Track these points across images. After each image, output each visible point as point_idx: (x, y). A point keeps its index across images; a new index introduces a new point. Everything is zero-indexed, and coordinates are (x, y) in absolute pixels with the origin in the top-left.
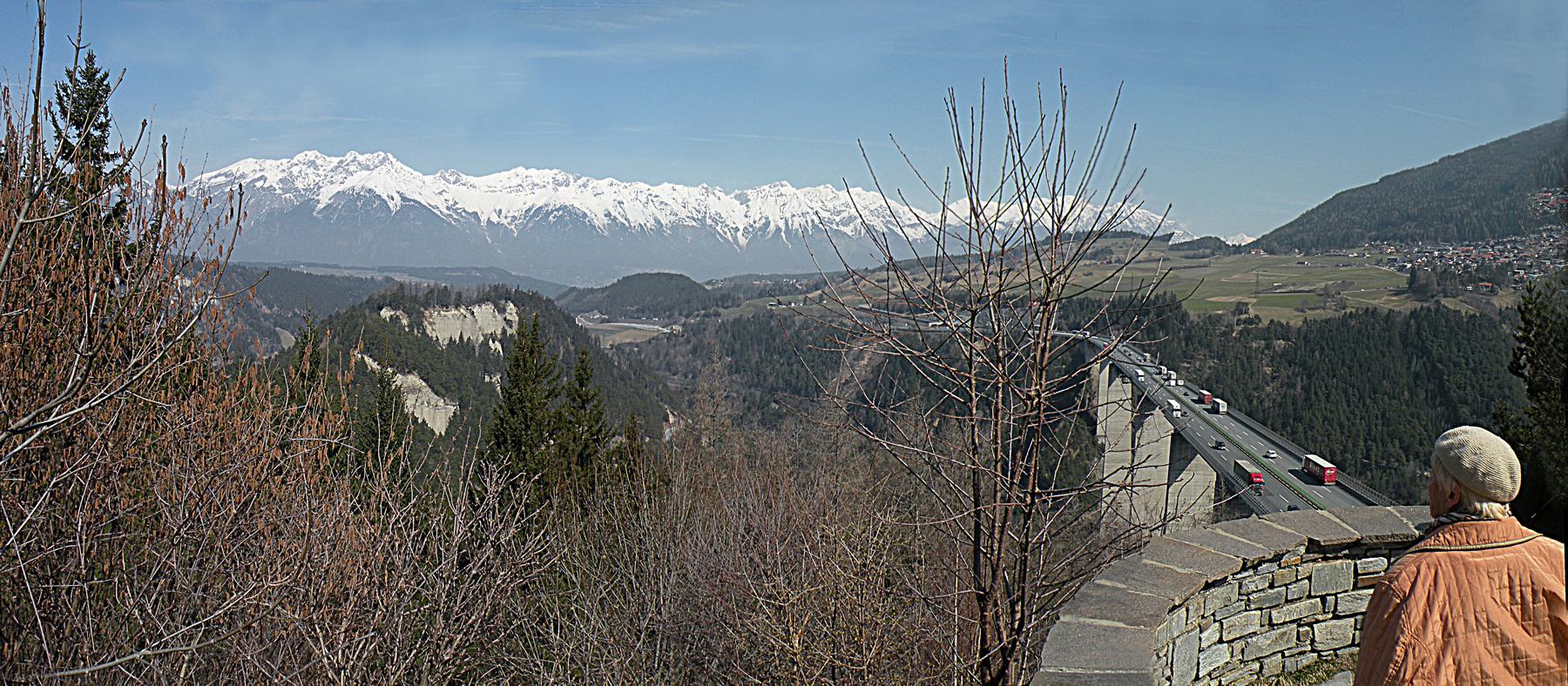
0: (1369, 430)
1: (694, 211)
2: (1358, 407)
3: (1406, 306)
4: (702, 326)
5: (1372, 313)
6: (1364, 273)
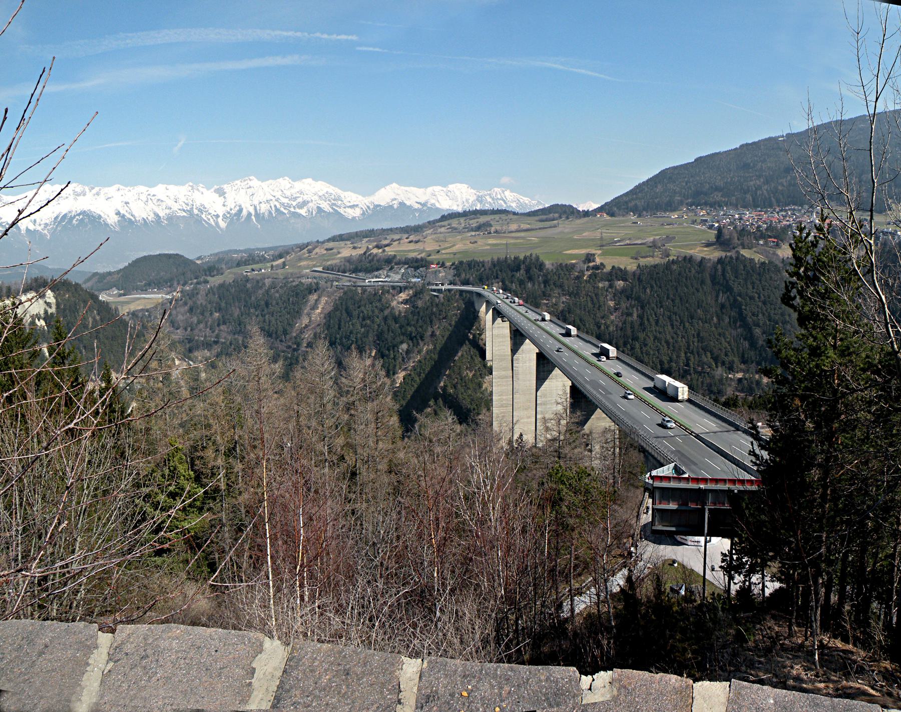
0: (689, 346)
1: (184, 204)
2: (679, 329)
3: (714, 254)
4: (195, 292)
5: (689, 260)
6: (682, 230)
